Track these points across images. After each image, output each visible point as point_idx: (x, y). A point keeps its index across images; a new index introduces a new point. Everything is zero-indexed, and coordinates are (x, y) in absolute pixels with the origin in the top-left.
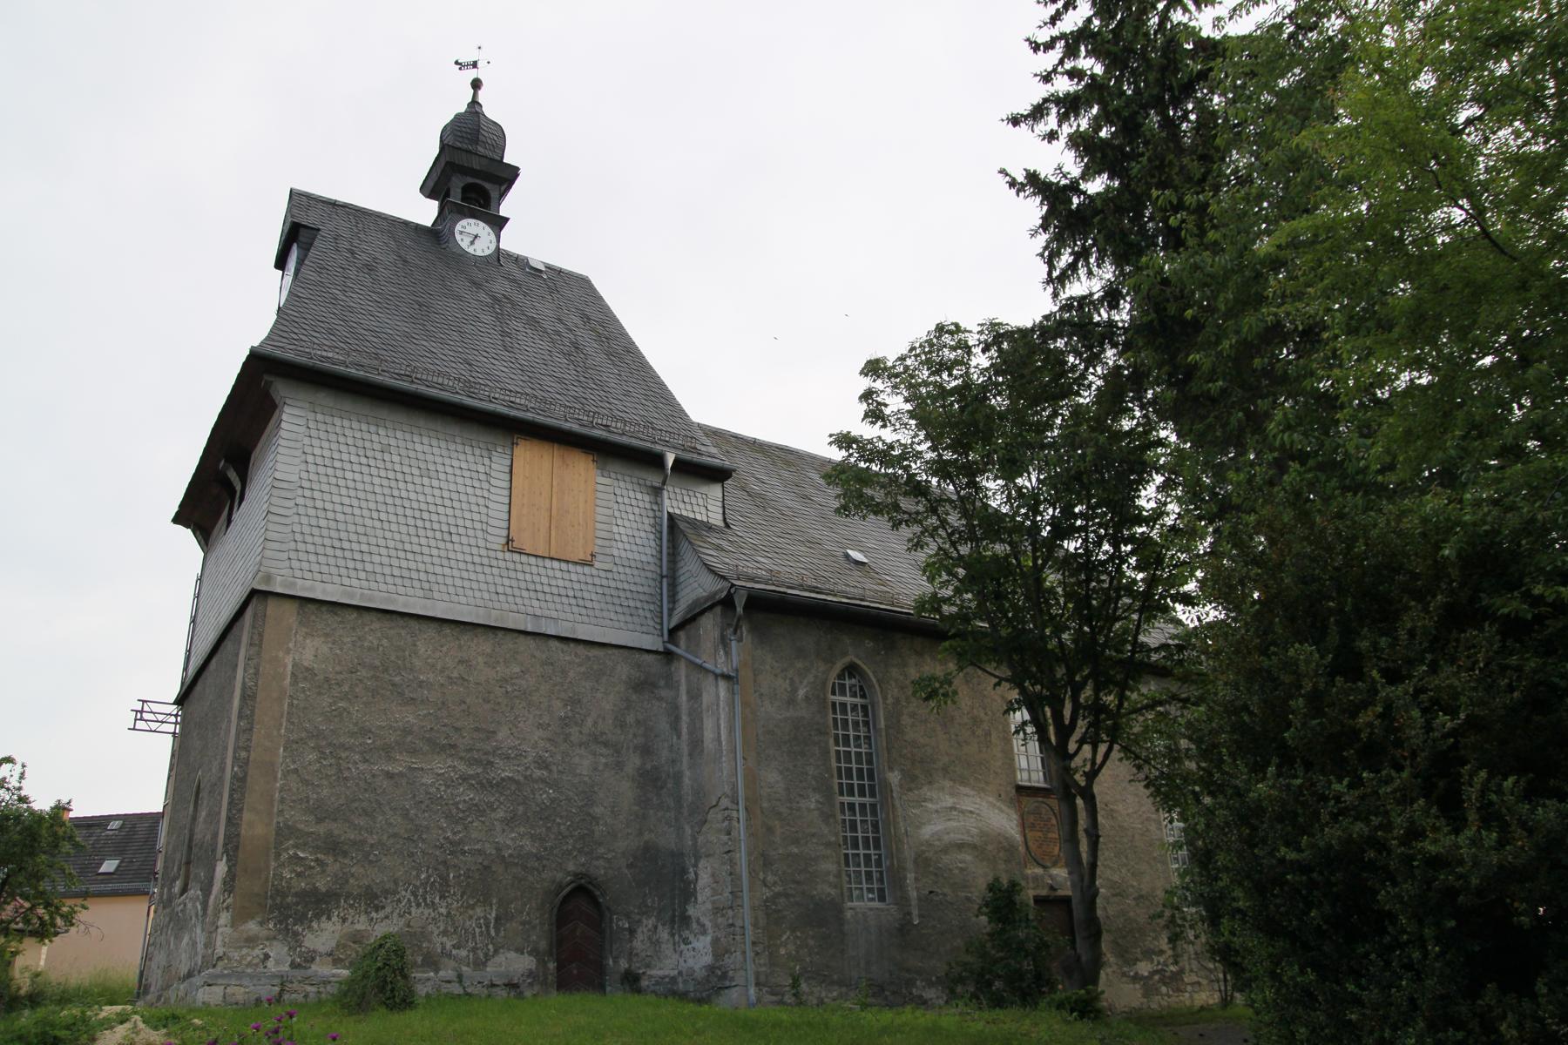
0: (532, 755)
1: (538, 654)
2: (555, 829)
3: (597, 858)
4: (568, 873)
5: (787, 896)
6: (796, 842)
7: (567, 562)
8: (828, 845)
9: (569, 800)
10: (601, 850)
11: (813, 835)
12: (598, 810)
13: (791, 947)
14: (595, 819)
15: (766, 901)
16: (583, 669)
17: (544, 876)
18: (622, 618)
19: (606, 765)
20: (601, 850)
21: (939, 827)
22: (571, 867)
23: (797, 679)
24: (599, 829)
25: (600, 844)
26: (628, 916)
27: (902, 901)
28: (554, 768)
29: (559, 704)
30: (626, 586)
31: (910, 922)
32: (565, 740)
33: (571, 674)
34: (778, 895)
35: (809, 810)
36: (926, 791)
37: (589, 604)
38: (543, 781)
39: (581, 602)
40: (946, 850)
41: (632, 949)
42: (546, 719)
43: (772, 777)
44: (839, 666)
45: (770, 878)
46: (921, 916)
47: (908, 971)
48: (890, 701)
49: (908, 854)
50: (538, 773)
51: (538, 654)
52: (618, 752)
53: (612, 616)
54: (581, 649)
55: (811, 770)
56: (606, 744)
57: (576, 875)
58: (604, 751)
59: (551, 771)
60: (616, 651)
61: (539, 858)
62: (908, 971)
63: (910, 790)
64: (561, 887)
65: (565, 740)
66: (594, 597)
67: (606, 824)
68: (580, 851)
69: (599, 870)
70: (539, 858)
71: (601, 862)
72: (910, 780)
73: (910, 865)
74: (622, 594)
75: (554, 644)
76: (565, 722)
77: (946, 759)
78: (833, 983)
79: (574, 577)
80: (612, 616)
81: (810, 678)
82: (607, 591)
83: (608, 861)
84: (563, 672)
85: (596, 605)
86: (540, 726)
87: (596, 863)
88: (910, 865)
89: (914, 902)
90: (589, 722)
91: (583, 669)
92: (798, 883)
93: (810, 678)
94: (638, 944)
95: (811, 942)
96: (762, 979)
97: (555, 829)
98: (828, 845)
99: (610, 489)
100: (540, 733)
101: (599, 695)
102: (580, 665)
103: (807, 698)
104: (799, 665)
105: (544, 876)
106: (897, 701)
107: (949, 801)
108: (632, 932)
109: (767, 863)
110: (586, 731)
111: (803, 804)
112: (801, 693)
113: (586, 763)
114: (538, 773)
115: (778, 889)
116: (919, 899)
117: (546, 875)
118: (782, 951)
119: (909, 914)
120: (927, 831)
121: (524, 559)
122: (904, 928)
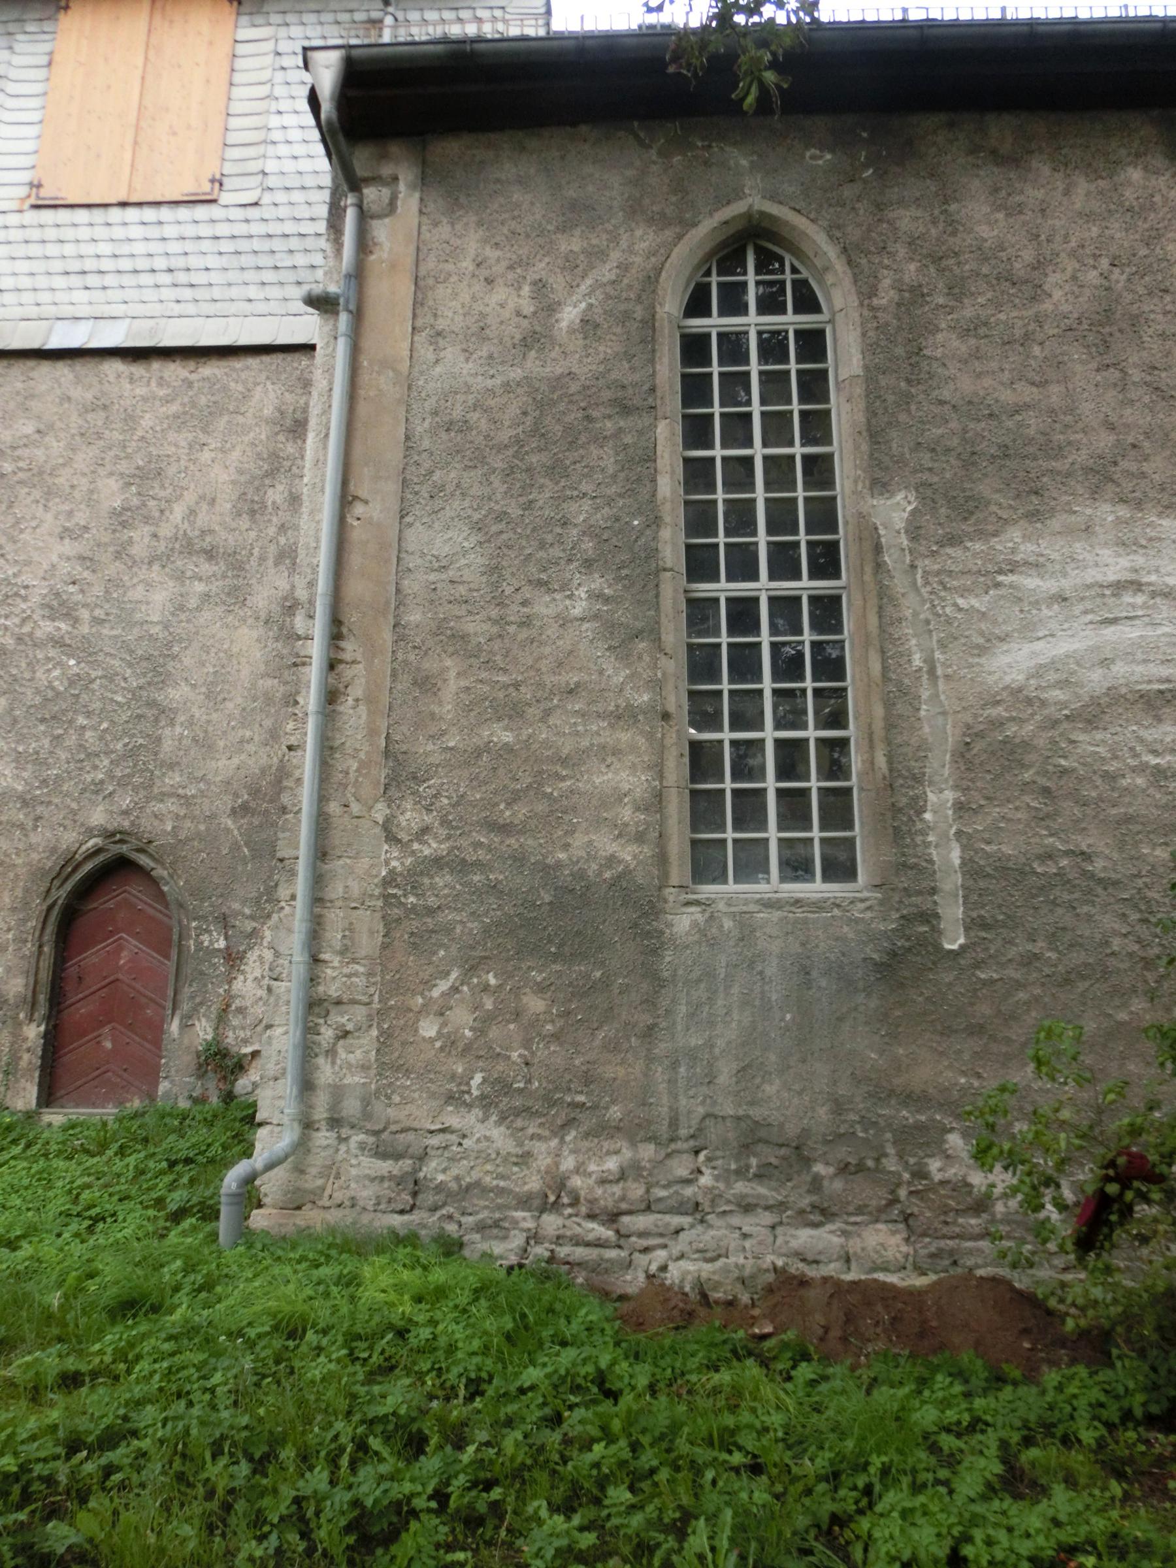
0: (40, 591)
1: (76, 393)
2: (72, 740)
3: (162, 797)
4: (90, 832)
5: (462, 867)
6: (513, 712)
7: (157, 204)
8: (625, 716)
9: (110, 677)
10: (174, 779)
11: (571, 692)
12: (176, 694)
13: (462, 1019)
14: (164, 713)
15: (390, 880)
16: (174, 408)
17: (34, 838)
18: (275, 292)
19: (206, 596)
20: (174, 779)
21: (1064, 646)
22: (98, 817)
23: (558, 282)
24: (171, 738)
25: (172, 766)
26: (224, 921)
27: (909, 874)
28: (85, 614)
29: (113, 484)
30: (289, 228)
31: (930, 945)
32: (118, 555)
33: (147, 421)
34: (437, 862)
35: (564, 621)
36: (1015, 540)
37: (199, 278)
38: (58, 642)
39: (182, 278)
40: (1092, 714)
41: (229, 998)
42: (81, 518)
43: (446, 544)
44: (706, 229)
45: (410, 817)
46: (970, 925)
47: (910, 1099)
48: (886, 296)
49: (938, 726)
50: (47, 627)
51: (76, 393)
52: (238, 567)
53: (253, 292)
54: (175, 371)
55: (580, 511)
56: (210, 554)
57: (109, 835)
58: (206, 568)
59: (76, 621)
60: (253, 362)
61: (25, 802)
62: (910, 1099)
63: (953, 540)
64: (70, 863)
65: (118, 555)
66: (212, 261)
67: (191, 722)
68: (123, 783)
69: (161, 820)
70: (25, 802)
71: (171, 805)
72: (955, 511)
73: (941, 764)
74: (277, 244)
75: (115, 367)
76: (122, 518)
77: (1105, 441)
78: (605, 1130)
79: (170, 231)
80: (253, 292)
81: (606, 272)
82: (243, 245)
83: (187, 801)
84: (130, 419)
85: (214, 277)
86: (66, 533)
87: (157, 807)
88: (941, 764)
89: (952, 882)
90: (178, 512)
91: (174, 408)
92: (505, 829)
93: (606, 272)
94: (247, 986)
95: (535, 1004)
96: (351, 1107)
97: (72, 740)
98: (625, 716)
99: (269, 46)
100: (68, 547)
101: (206, 456)
102: (167, 401)
103: (588, 325)
104: (572, 243)
105: (34, 838)
106: (915, 295)
107: (1114, 565)
108: (233, 959)
109: (400, 774)
110: (166, 531)
111: (544, 606)
112: (570, 315)
113: (159, 597)
114: (47, 627)
115: (431, 848)
116: (971, 869)
117: (41, 837)
118: (429, 1029)
119: (930, 917)
120: (1012, 663)
121: (63, 215)
122: (902, 962)
